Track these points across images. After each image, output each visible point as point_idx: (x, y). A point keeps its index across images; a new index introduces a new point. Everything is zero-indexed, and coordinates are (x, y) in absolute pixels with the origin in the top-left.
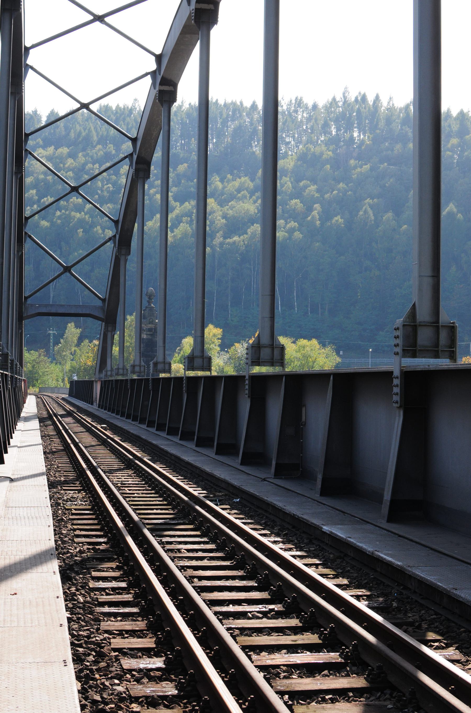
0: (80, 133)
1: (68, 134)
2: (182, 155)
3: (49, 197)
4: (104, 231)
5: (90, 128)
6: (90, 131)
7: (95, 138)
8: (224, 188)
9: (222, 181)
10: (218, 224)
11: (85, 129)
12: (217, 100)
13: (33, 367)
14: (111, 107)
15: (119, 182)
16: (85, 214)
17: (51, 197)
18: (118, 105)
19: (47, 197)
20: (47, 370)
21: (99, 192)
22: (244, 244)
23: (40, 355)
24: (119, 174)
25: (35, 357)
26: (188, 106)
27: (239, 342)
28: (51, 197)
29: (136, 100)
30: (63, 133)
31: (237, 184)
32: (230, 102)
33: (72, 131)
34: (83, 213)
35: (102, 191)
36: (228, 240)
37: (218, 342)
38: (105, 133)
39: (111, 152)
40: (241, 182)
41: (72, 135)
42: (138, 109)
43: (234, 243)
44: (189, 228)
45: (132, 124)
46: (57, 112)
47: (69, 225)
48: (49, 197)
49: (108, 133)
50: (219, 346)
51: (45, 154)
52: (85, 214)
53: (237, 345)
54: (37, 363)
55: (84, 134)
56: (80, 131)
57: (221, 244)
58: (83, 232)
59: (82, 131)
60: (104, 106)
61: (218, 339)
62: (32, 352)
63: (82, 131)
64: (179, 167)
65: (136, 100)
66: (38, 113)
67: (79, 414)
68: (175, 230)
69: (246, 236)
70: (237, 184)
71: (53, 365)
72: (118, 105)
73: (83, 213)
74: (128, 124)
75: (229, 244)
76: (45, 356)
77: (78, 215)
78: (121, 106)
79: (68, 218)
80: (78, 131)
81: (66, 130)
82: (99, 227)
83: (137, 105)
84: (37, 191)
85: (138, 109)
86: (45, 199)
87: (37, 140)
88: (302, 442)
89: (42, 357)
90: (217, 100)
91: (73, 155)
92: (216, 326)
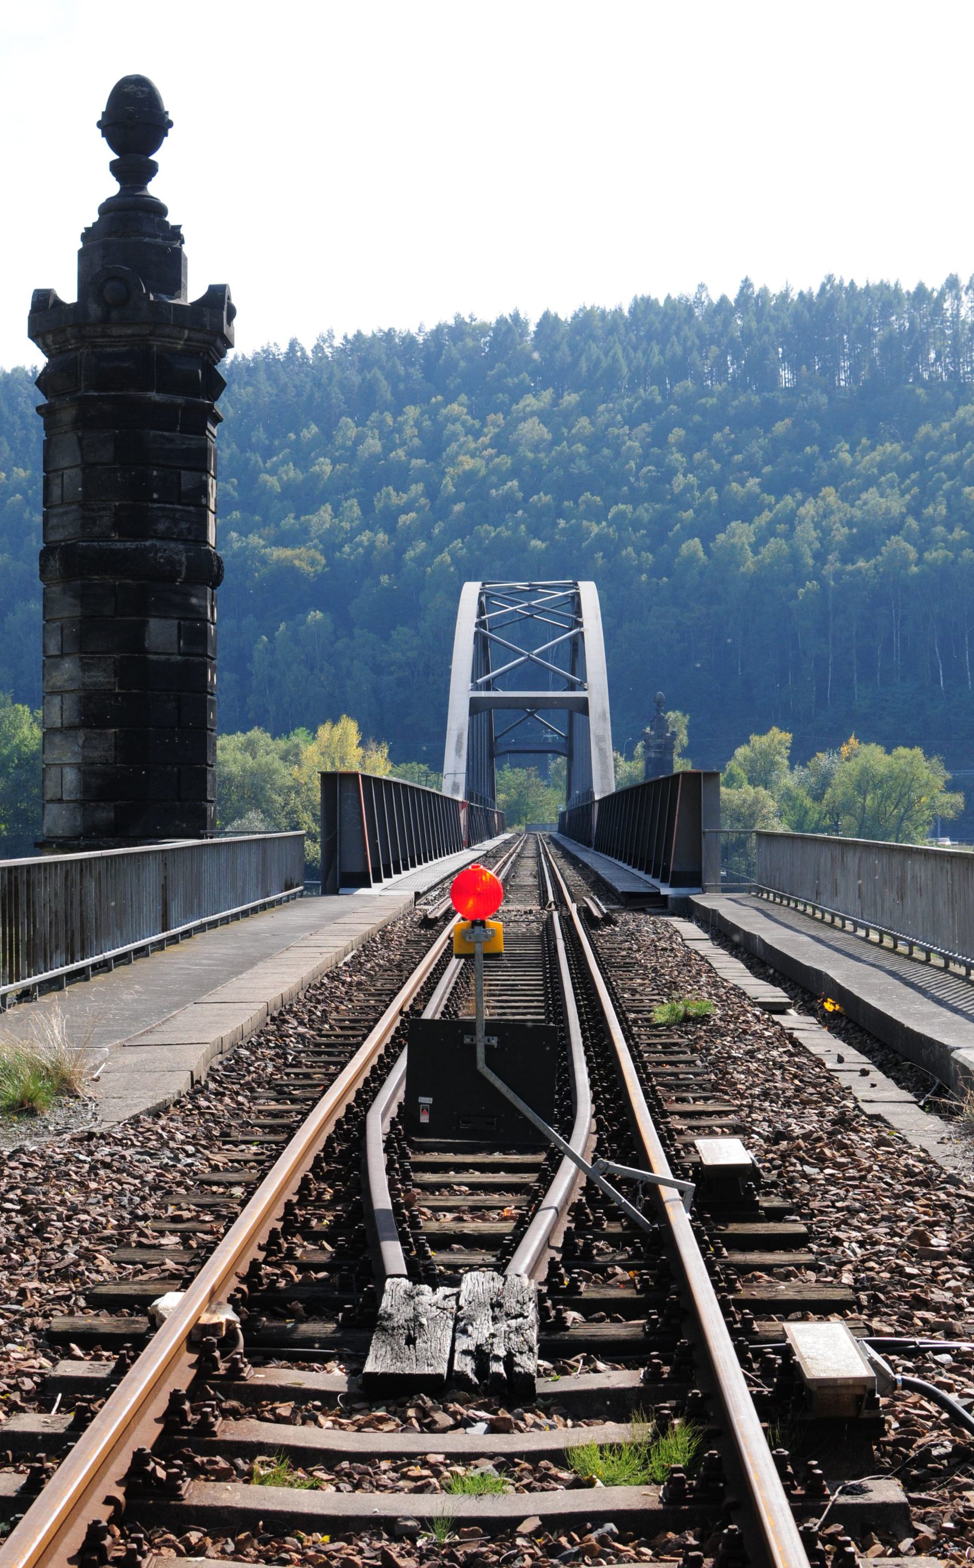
0: (598, 361)
1: (576, 362)
2: (781, 401)
3: (542, 494)
4: (639, 554)
5: (615, 353)
6: (615, 359)
7: (625, 370)
8: (855, 463)
9: (852, 451)
10: (835, 536)
11: (606, 354)
12: (852, 283)
13: (520, 794)
14: (656, 300)
15: (667, 460)
16: (609, 526)
17: (546, 494)
18: (669, 297)
19: (538, 493)
20: (540, 798)
21: (632, 479)
22: (878, 572)
23: (529, 776)
24: (667, 443)
25: (522, 779)
26: (796, 298)
27: (822, 751)
28: (546, 494)
29: (702, 286)
30: (569, 359)
31: (876, 456)
32: (877, 283)
33: (583, 358)
34: (604, 523)
35: (637, 479)
36: (849, 568)
37: (786, 753)
38: (643, 363)
39: (654, 400)
40: (884, 453)
41: (583, 365)
42: (706, 303)
43: (859, 571)
44: (784, 546)
45: (693, 342)
46: (556, 315)
47: (581, 544)
48: (542, 494)
49: (648, 360)
50: (789, 758)
51: (535, 408)
52: (609, 526)
53: (819, 754)
54: (526, 788)
55: (604, 365)
56: (598, 357)
57: (837, 576)
58: (603, 558)
59: (602, 357)
60: (642, 299)
61: (787, 748)
62: (517, 770)
63: (602, 357)
64: (777, 425)
65: (702, 286)
66: (522, 316)
67: (600, 904)
68: (761, 549)
69: (879, 558)
70: (876, 456)
71: (551, 790)
72: (669, 297)
73: (604, 523)
74: (686, 339)
75: (851, 574)
76: (536, 776)
77: (595, 529)
78: (675, 296)
79: (576, 534)
80: (594, 357)
81: (572, 355)
82: (630, 549)
83: (704, 295)
84: (521, 482)
85: (706, 303)
86: (535, 497)
87: (522, 376)
88: (859, 879)
89: (533, 779)
90: (852, 283)
91: (586, 409)
92: (783, 729)
